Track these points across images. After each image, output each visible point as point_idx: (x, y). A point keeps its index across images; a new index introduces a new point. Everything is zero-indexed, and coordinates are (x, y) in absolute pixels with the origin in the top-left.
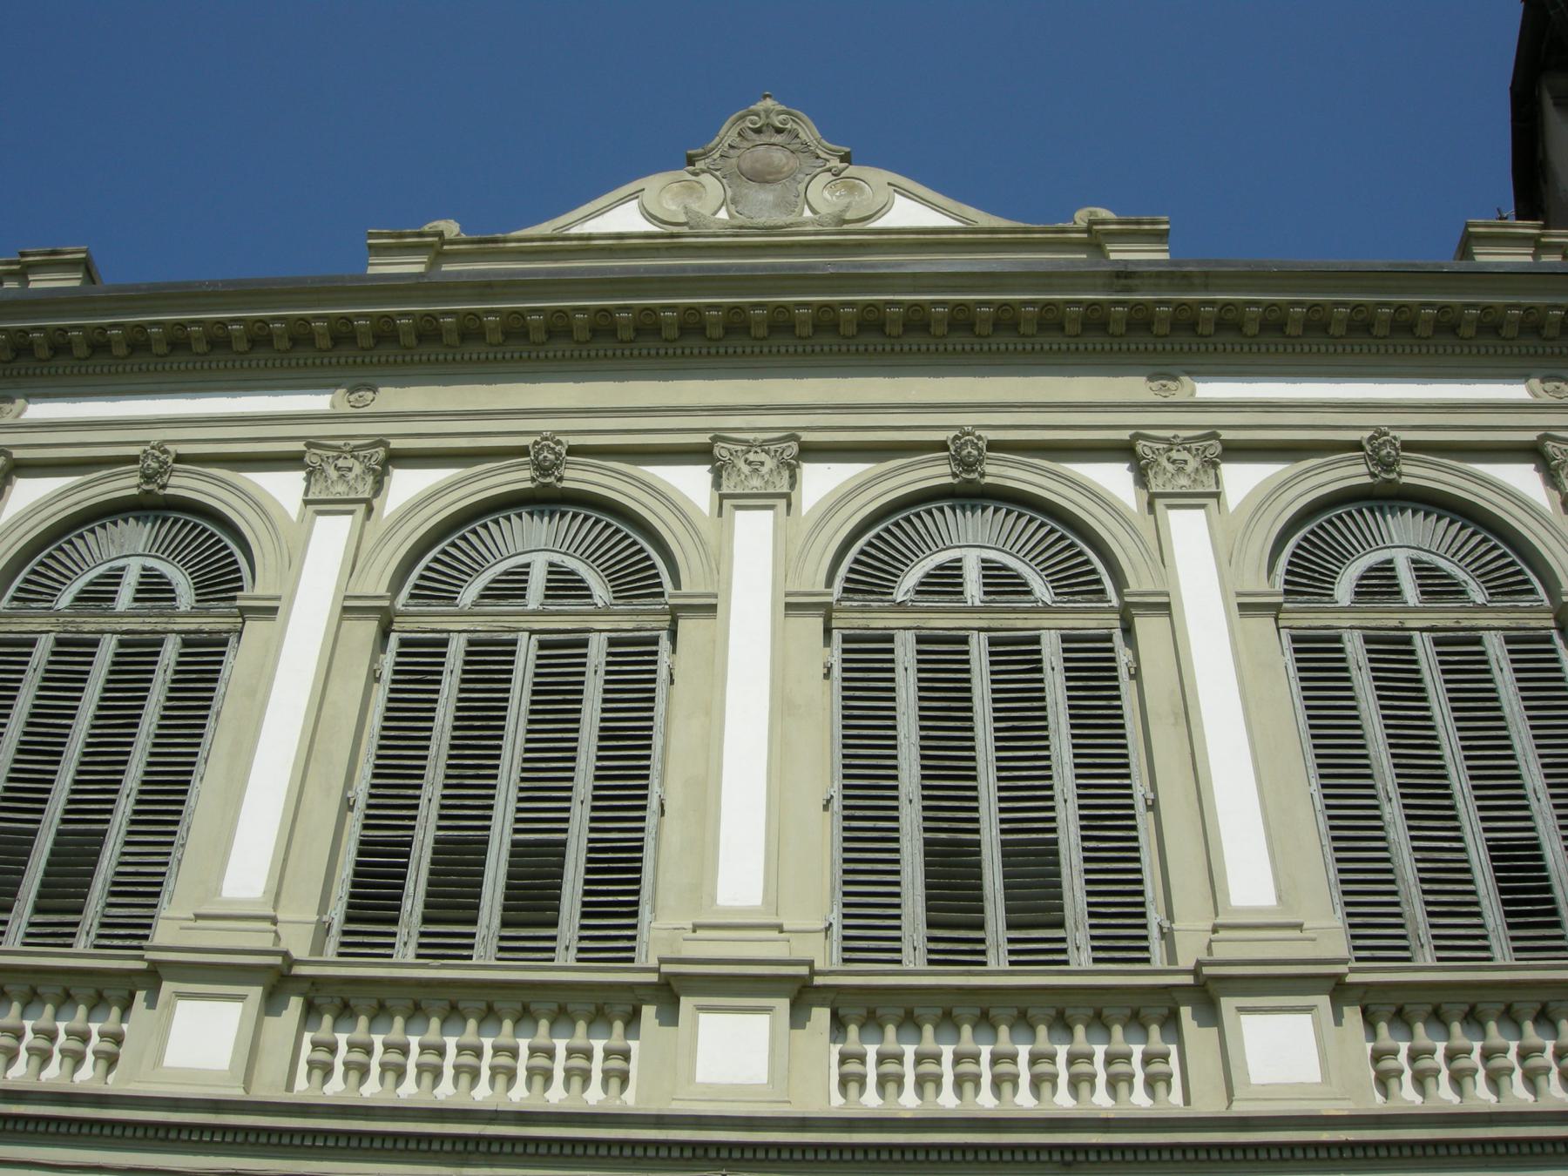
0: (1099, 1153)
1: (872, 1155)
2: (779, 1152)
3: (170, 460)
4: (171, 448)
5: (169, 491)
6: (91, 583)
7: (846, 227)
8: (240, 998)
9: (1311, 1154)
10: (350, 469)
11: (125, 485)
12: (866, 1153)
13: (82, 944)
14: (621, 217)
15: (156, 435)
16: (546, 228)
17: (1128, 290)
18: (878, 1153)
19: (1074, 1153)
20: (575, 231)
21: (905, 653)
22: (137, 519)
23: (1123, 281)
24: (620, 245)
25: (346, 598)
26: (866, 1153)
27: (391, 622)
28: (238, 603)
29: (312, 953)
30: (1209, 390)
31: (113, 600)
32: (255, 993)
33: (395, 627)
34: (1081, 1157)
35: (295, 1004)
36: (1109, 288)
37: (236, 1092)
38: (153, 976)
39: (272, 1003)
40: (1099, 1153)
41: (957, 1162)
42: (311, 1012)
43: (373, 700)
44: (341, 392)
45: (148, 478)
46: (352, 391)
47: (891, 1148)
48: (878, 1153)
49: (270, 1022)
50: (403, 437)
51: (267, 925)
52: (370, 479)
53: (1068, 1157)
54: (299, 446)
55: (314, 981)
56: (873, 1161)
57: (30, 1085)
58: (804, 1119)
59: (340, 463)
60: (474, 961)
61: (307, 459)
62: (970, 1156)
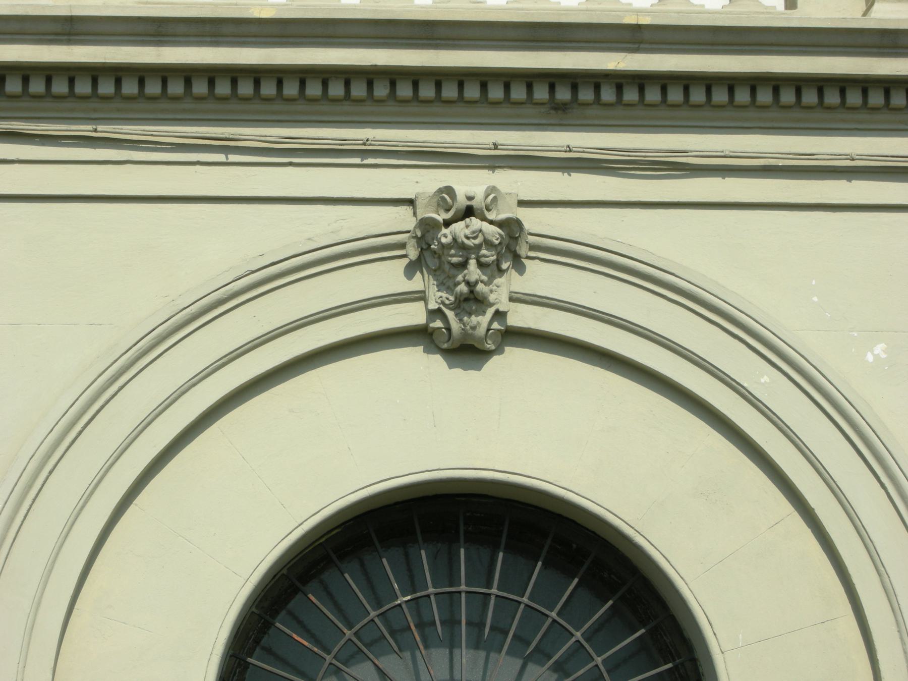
0: (619, 88)
1: (200, 88)
2: (142, 82)
9: (496, 92)
12: (188, 83)
18: (211, 83)
19: (575, 88)
21: (324, 655)
26: (188, 83)
34: (587, 95)
38: (336, 566)
40: (619, 88)
41: (176, 99)
43: (455, 660)
47: (234, 73)
48: (211, 83)
53: (563, 94)
56: (200, 99)
58: (70, 20)
62: (381, 90)
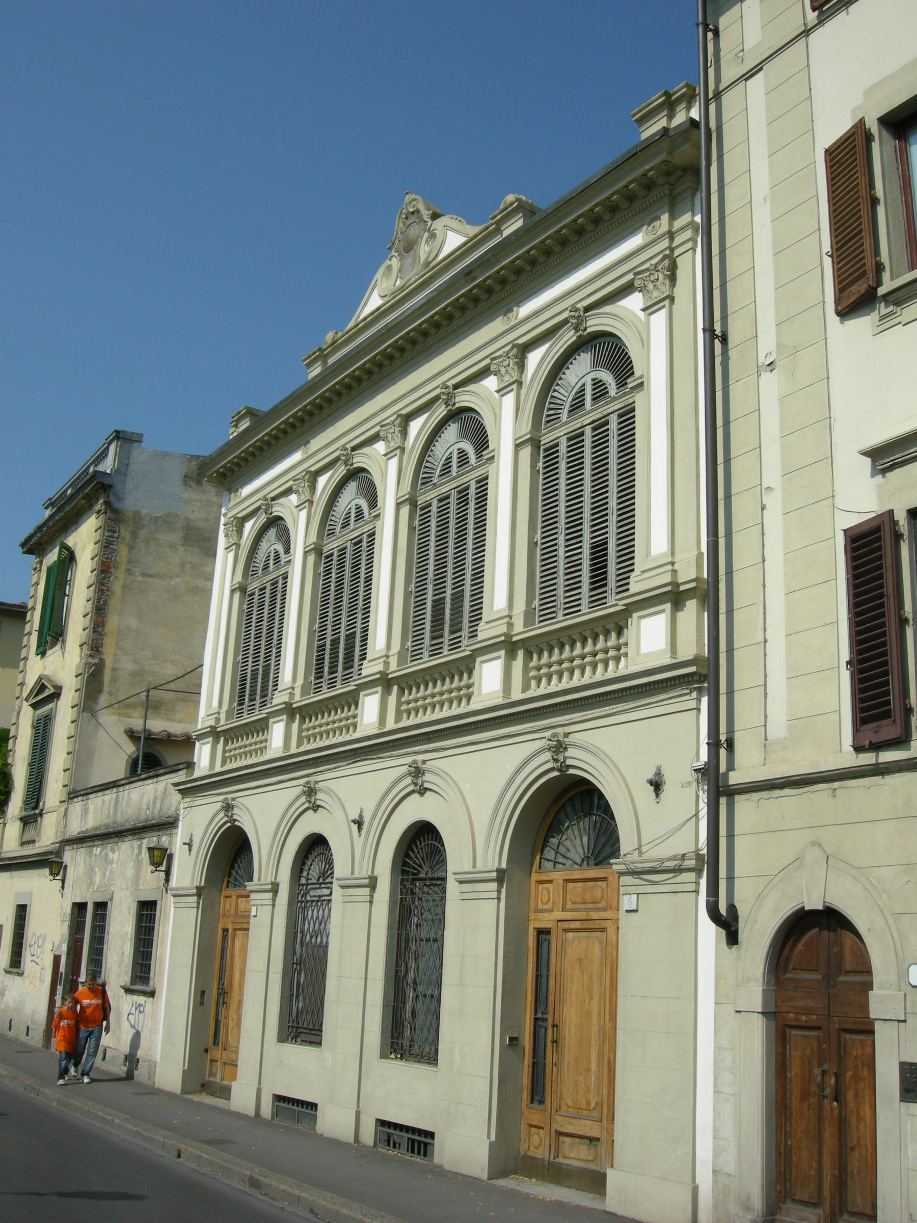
3: (582, 313)
4: (579, 306)
5: (589, 330)
6: (574, 400)
7: (431, 265)
8: (663, 611)
10: (658, 280)
11: (568, 337)
13: (584, 608)
14: (374, 302)
15: (261, 495)
16: (352, 323)
17: (474, 279)
20: (362, 317)
22: (583, 352)
23: (470, 276)
24: (379, 314)
25: (516, 439)
27: (540, 442)
28: (630, 386)
29: (525, 627)
30: (525, 310)
31: (607, 392)
32: (668, 606)
33: (542, 443)
35: (521, 654)
36: (468, 283)
37: (667, 661)
38: (628, 611)
39: (511, 655)
42: (529, 655)
44: (645, 228)
45: (576, 329)
46: (505, 315)
49: (680, 615)
50: (522, 335)
51: (670, 567)
52: (667, 282)
54: (630, 276)
55: (299, 708)
57: (558, 689)
59: (652, 278)
60: (632, 591)
61: (636, 284)
